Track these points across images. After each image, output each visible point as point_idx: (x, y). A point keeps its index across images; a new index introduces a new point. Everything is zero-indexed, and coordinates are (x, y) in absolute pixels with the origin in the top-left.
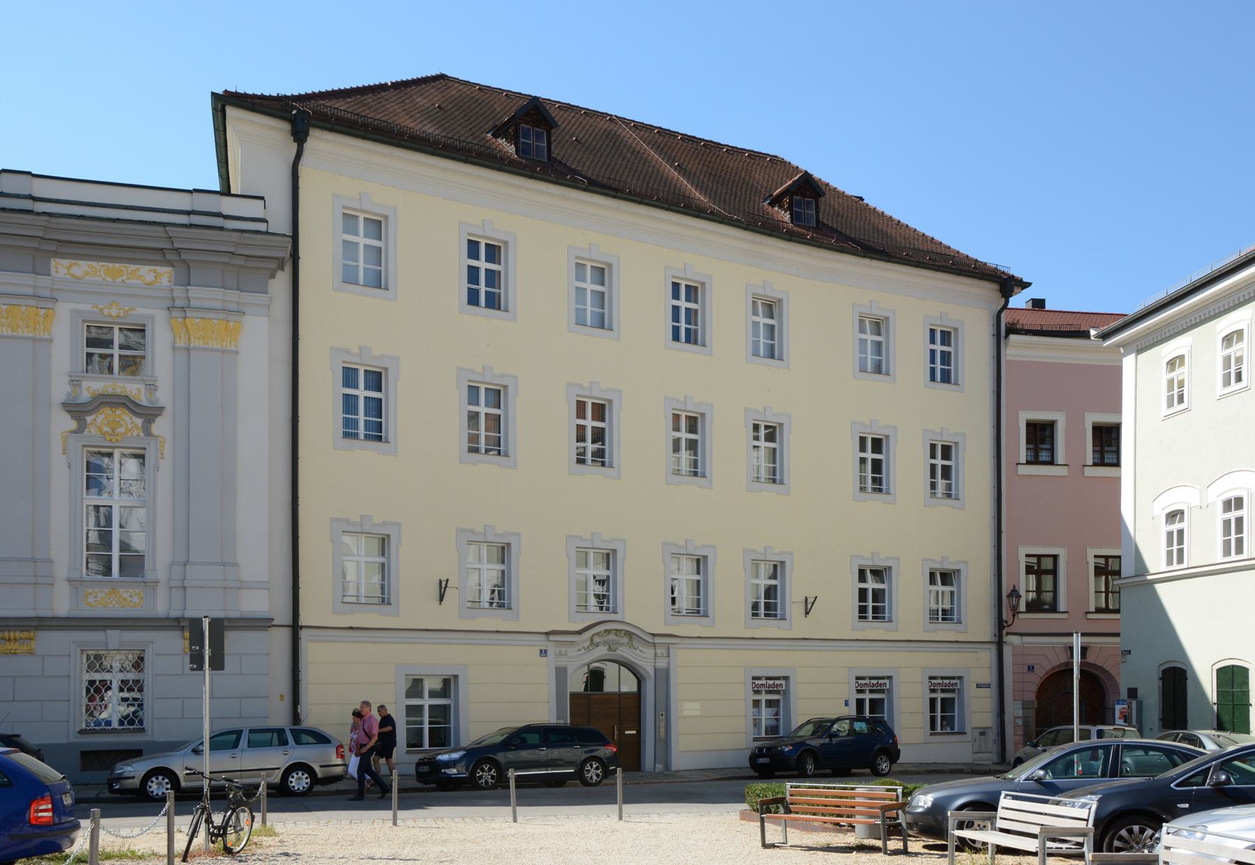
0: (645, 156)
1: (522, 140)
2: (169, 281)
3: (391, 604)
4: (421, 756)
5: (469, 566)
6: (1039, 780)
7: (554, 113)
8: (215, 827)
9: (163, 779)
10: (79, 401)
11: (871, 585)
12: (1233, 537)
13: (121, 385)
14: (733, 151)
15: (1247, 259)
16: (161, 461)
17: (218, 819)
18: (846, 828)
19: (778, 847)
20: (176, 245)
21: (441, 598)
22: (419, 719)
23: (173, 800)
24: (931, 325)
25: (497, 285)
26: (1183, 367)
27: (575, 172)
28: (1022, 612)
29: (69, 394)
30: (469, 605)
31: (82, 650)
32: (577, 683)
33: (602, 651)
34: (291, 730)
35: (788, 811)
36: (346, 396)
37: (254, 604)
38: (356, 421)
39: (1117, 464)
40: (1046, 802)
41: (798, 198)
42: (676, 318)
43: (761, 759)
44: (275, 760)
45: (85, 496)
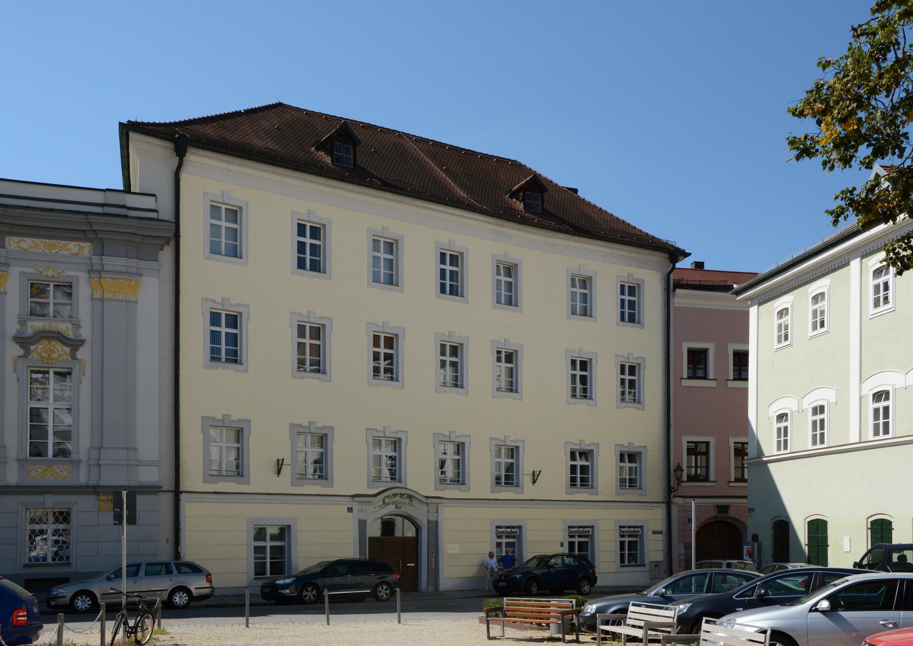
0: (423, 162)
1: (335, 153)
2: (89, 252)
3: (243, 476)
4: (265, 581)
5: (298, 449)
6: (663, 595)
7: (358, 134)
8: (129, 627)
9: (86, 598)
10: (25, 336)
11: (579, 463)
12: (881, 421)
13: (55, 324)
14: (486, 157)
15: (843, 237)
16: (83, 377)
17: (131, 623)
18: (545, 627)
19: (498, 639)
20: (95, 228)
21: (279, 472)
22: (263, 556)
23: (105, 609)
24: (621, 282)
25: (318, 255)
26: (824, 301)
27: (372, 176)
28: (684, 482)
29: (18, 331)
30: (298, 476)
31: (27, 509)
32: (374, 530)
33: (391, 509)
34: (175, 563)
35: (505, 616)
36: (212, 332)
37: (148, 476)
38: (220, 349)
39: (747, 379)
40: (661, 608)
41: (530, 193)
42: (443, 277)
43: (500, 583)
44: (164, 584)
45: (29, 401)
